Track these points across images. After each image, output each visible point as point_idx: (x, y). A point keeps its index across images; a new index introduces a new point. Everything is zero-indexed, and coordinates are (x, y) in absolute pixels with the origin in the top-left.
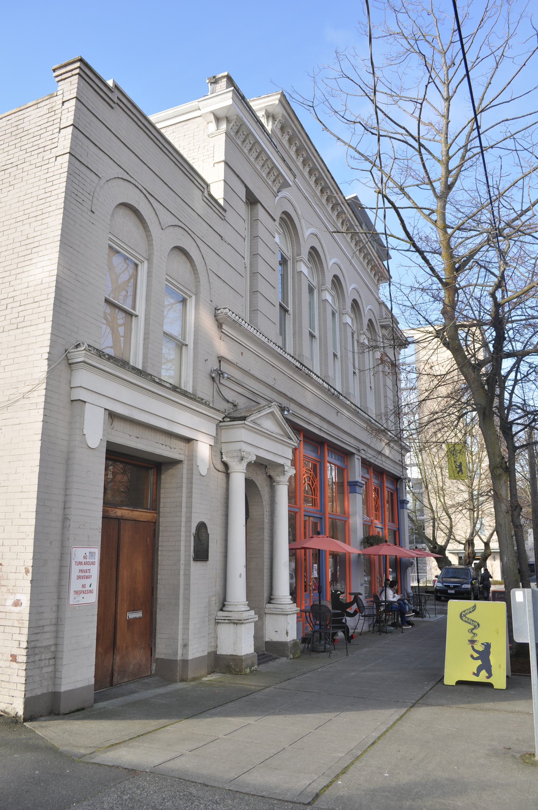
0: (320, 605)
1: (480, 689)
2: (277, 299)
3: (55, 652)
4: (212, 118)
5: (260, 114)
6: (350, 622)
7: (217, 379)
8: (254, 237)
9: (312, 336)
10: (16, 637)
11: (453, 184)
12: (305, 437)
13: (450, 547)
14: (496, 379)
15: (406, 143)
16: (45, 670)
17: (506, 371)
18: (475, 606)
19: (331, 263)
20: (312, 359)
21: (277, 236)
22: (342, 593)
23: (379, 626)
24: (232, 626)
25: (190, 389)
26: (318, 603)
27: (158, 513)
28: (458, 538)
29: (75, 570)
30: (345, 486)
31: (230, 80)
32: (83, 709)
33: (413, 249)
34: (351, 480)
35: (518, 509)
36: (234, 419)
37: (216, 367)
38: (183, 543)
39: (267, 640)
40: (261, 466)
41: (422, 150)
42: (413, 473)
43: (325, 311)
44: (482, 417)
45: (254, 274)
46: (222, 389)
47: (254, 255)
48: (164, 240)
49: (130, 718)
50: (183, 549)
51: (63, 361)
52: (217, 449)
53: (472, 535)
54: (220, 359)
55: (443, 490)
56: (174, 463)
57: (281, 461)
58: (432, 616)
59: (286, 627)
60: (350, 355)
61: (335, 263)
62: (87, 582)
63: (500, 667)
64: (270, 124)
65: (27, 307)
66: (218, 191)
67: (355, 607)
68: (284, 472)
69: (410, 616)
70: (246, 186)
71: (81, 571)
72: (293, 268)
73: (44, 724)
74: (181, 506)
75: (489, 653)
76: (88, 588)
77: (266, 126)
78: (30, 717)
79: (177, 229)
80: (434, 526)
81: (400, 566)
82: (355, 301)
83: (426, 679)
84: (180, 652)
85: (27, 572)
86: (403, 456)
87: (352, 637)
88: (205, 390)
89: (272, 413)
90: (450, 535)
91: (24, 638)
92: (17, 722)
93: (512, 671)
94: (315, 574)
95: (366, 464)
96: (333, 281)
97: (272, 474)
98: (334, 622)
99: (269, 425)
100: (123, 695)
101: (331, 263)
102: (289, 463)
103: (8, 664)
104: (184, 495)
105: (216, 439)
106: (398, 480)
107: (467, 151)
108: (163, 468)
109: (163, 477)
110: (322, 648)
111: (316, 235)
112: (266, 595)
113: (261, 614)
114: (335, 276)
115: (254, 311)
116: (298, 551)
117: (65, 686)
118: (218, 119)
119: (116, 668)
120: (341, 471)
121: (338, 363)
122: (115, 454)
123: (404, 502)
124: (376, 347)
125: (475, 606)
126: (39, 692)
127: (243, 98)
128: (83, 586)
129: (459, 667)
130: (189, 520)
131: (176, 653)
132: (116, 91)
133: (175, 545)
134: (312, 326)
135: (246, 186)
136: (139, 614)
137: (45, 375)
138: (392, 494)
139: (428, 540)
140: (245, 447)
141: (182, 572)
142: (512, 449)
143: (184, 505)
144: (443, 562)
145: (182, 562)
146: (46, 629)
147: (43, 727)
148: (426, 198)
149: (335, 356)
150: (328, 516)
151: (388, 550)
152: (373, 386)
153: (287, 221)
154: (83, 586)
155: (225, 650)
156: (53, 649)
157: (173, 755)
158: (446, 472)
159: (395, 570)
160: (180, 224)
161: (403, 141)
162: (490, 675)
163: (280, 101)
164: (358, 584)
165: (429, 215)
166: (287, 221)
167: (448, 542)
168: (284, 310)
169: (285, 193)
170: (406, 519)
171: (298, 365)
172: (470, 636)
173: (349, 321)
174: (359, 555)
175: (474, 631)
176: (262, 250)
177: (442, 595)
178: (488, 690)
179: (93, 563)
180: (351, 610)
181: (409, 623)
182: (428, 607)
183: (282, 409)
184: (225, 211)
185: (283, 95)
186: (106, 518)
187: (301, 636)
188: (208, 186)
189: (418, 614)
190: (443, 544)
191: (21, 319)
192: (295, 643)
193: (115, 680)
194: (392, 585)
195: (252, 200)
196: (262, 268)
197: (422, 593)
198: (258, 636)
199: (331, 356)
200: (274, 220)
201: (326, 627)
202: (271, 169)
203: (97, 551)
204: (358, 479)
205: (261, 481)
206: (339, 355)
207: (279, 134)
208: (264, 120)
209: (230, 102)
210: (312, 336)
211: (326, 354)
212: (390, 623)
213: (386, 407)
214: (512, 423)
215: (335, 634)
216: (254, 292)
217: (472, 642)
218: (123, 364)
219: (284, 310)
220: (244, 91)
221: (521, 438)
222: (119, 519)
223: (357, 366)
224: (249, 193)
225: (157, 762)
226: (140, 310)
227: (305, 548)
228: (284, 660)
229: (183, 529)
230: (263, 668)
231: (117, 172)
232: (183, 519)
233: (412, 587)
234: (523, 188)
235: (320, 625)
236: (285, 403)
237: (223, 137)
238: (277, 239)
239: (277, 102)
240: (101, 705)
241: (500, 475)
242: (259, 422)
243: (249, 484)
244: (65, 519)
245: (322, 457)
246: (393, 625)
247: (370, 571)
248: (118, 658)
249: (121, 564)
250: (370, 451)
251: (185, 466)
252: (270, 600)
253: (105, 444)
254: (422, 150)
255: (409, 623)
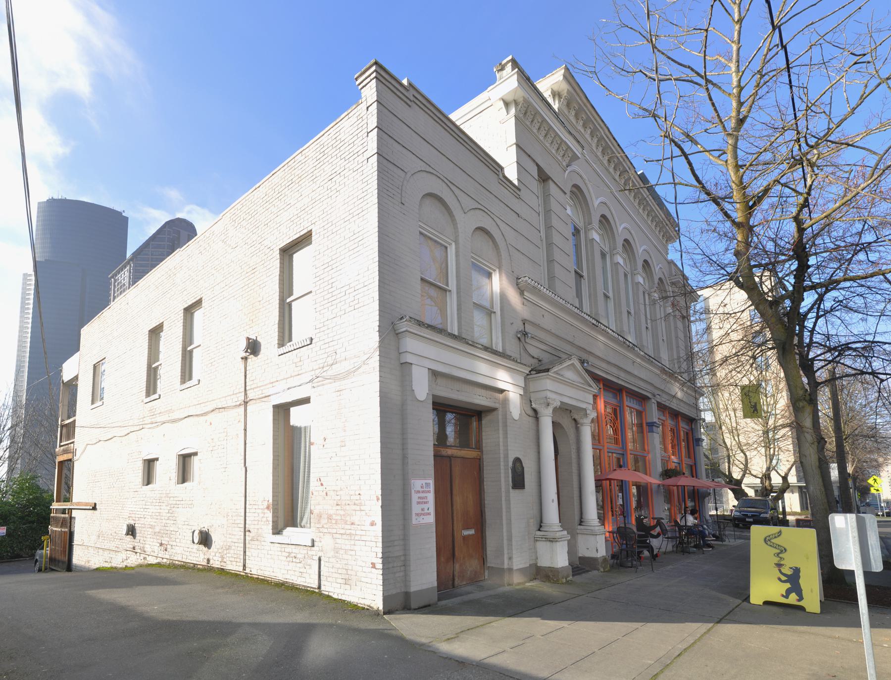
0: (625, 527)
1: (790, 610)
2: (572, 267)
3: (405, 560)
4: (501, 104)
5: (547, 95)
6: (655, 543)
7: (522, 339)
8: (548, 212)
9: (606, 297)
10: (374, 549)
11: (745, 117)
12: (604, 385)
13: (745, 481)
14: (796, 317)
15: (691, 81)
16: (397, 575)
17: (805, 309)
18: (780, 532)
19: (620, 229)
20: (608, 317)
21: (568, 208)
22: (645, 518)
23: (682, 548)
24: (548, 543)
25: (500, 349)
26: (623, 525)
27: (482, 452)
28: (754, 472)
29: (415, 498)
30: (645, 427)
31: (515, 63)
32: (429, 606)
33: (704, 196)
34: (649, 421)
35: (823, 442)
36: (539, 372)
37: (521, 328)
38: (502, 475)
39: (581, 555)
40: (564, 410)
41: (710, 86)
42: (708, 417)
43: (617, 273)
44: (781, 352)
45: (550, 245)
46: (529, 348)
47: (549, 227)
48: (467, 222)
49: (464, 615)
50: (503, 480)
51: (391, 328)
52: (527, 397)
53: (768, 469)
54: (524, 322)
55: (737, 430)
56: (492, 410)
57: (584, 406)
58: (732, 540)
59: (597, 545)
60: (642, 307)
61: (624, 228)
62: (425, 506)
63: (812, 591)
64: (557, 102)
65: (360, 291)
66: (512, 173)
67: (658, 529)
68: (586, 415)
69: (710, 539)
70: (537, 165)
71: (419, 498)
72: (586, 237)
73: (398, 616)
74: (499, 445)
75: (799, 577)
76: (426, 511)
77: (552, 104)
78: (388, 611)
79: (478, 211)
80: (729, 462)
81: (698, 497)
82: (646, 261)
83: (729, 598)
84: (506, 561)
85: (378, 499)
86: (697, 399)
87: (657, 555)
88: (513, 348)
89: (573, 364)
90: (746, 470)
91: (380, 550)
92: (379, 614)
93: (825, 596)
94: (620, 502)
95: (662, 407)
96: (623, 245)
97: (576, 417)
98: (639, 542)
99: (570, 375)
100: (461, 595)
101: (620, 229)
102: (590, 407)
103: (370, 569)
104: (501, 436)
105: (525, 389)
106: (693, 421)
107: (762, 76)
108: (483, 415)
109: (483, 422)
110: (630, 564)
111: (605, 204)
112: (577, 518)
113: (573, 535)
114: (626, 240)
115: (551, 278)
116: (604, 482)
117: (414, 588)
118: (507, 104)
119: (456, 573)
120: (640, 414)
121: (632, 319)
122: (441, 407)
123: (699, 441)
124: (667, 297)
125: (780, 532)
126: (394, 592)
127: (528, 79)
128: (423, 510)
129: (765, 587)
130: (506, 456)
131: (503, 563)
132: (412, 92)
133: (497, 478)
134: (606, 288)
135: (537, 165)
136: (472, 532)
137: (377, 344)
138: (687, 433)
139: (725, 474)
140: (549, 395)
141: (503, 499)
142: (815, 385)
143: (501, 444)
144: (739, 493)
145: (503, 490)
146: (396, 543)
147: (396, 619)
148: (717, 139)
149: (629, 313)
150: (629, 452)
151: (686, 481)
152: (665, 338)
153: (577, 193)
154: (423, 510)
155: (544, 562)
156: (402, 558)
157: (497, 650)
158: (740, 414)
159: (693, 500)
160: (480, 207)
161: (688, 81)
162: (801, 598)
163: (564, 76)
164: (661, 509)
165: (719, 156)
166: (577, 193)
167: (744, 476)
168: (579, 276)
169: (575, 167)
170: (702, 456)
171: (595, 322)
172: (776, 560)
173: (641, 280)
174: (659, 485)
175: (781, 555)
176: (555, 222)
177: (741, 522)
178: (800, 613)
179: (429, 492)
180: (654, 533)
181: (709, 546)
182: (727, 533)
183: (582, 362)
184: (519, 190)
185: (567, 69)
186: (436, 456)
187: (610, 553)
188: (502, 168)
189: (718, 538)
190: (739, 478)
191: (356, 302)
192: (605, 560)
193: (456, 583)
194: (693, 513)
195: (544, 178)
196: (557, 239)
197: (721, 520)
198: (572, 551)
199: (625, 315)
200: (565, 193)
201: (631, 548)
202: (560, 145)
203: (431, 482)
204: (655, 420)
205: (566, 423)
206: (632, 312)
207: (566, 111)
208: (550, 100)
209: (516, 84)
210: (606, 297)
211: (621, 313)
212: (692, 545)
213: (678, 352)
214: (813, 359)
215: (640, 553)
216: (550, 261)
217: (779, 565)
218: (441, 331)
219: (579, 276)
220: (528, 72)
221: (822, 375)
222: (450, 457)
223: (649, 317)
224: (540, 169)
225: (483, 656)
226: (452, 285)
227: (610, 480)
228: (595, 572)
229: (502, 464)
230: (578, 579)
231: (421, 166)
232: (502, 456)
233: (711, 516)
234: (831, 104)
235: (626, 544)
236: (585, 356)
237: (513, 120)
238: (569, 211)
239: (562, 78)
240: (443, 603)
241: (803, 407)
242: (562, 373)
243: (555, 424)
244: (404, 457)
245: (621, 401)
246: (695, 547)
247: (669, 498)
248: (457, 566)
249: (454, 492)
250: (664, 395)
251: (500, 412)
252: (581, 522)
253: (431, 397)
254: (710, 86)
255: (709, 546)
